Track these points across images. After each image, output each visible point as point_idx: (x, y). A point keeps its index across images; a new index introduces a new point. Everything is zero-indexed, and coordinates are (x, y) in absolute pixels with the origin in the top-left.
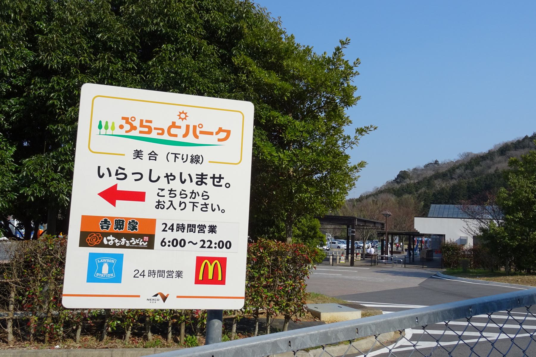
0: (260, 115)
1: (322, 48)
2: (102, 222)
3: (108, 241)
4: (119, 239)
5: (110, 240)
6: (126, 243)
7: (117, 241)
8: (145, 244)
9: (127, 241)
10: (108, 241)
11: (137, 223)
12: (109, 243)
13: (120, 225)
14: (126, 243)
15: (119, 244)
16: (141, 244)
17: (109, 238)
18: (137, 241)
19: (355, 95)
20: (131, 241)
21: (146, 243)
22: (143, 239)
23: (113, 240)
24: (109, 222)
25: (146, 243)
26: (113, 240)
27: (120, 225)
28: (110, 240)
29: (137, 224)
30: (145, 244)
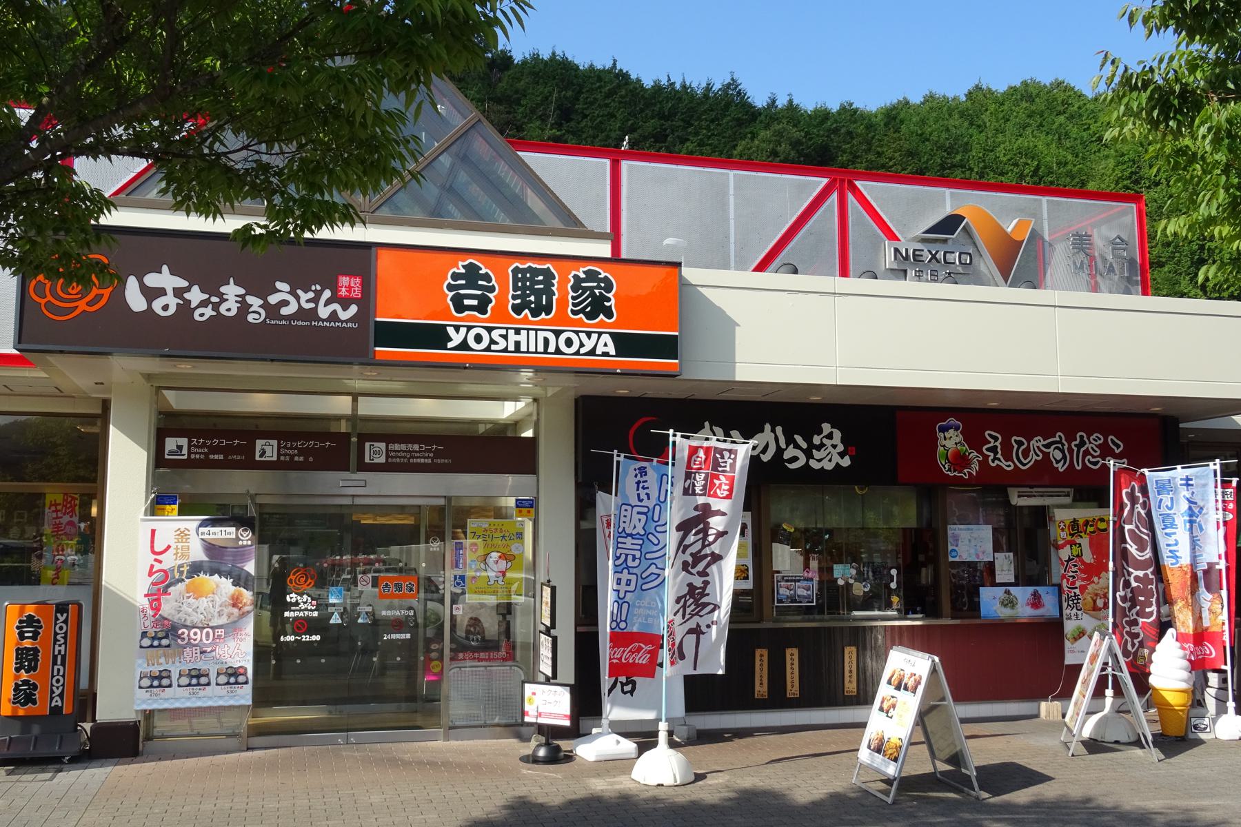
0: (829, 130)
1: (609, 65)
2: (456, 276)
3: (151, 294)
4: (212, 288)
5: (161, 292)
6: (244, 308)
7: (195, 296)
8: (344, 315)
9: (250, 299)
10: (151, 294)
11: (609, 288)
12: (157, 305)
13: (538, 294)
14: (244, 308)
15: (209, 312)
16: (324, 312)
17: (152, 280)
18: (304, 296)
19: (664, 82)
20: (273, 299)
21: (353, 309)
22: (335, 289)
23: (178, 292)
24: (487, 278)
25: (353, 309)
26: (178, 292)
27: (538, 294)
28: (161, 292)
29: (609, 289)
30: (344, 315)
